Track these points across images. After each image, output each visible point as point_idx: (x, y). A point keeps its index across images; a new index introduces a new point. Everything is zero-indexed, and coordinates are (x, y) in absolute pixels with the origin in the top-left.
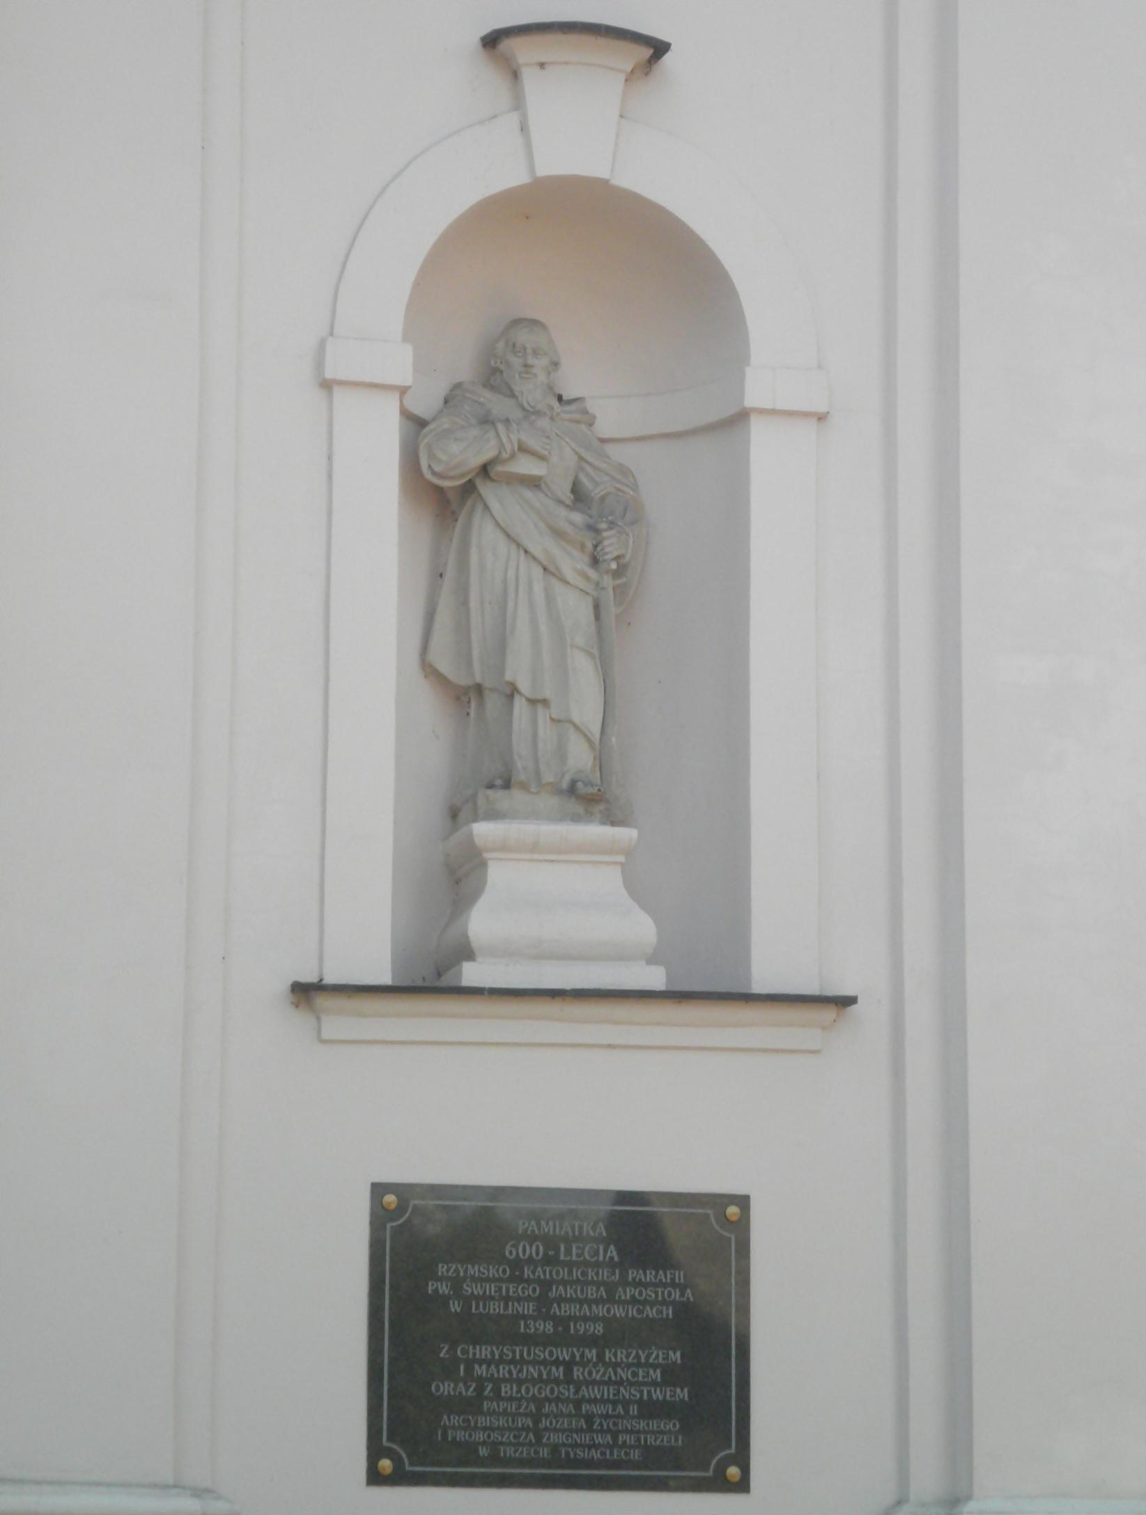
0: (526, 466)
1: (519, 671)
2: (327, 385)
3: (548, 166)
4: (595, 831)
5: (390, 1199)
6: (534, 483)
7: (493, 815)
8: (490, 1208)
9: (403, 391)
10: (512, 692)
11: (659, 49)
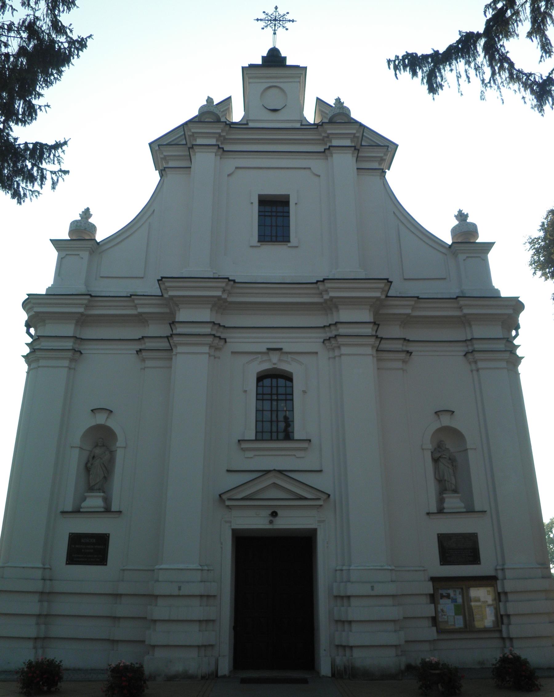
0: (444, 456)
1: (446, 478)
2: (423, 449)
3: (443, 425)
4: (456, 495)
5: (439, 535)
6: (445, 458)
7: (445, 494)
8: (387, 156)
9: (431, 449)
10: (445, 480)
11: (453, 412)
